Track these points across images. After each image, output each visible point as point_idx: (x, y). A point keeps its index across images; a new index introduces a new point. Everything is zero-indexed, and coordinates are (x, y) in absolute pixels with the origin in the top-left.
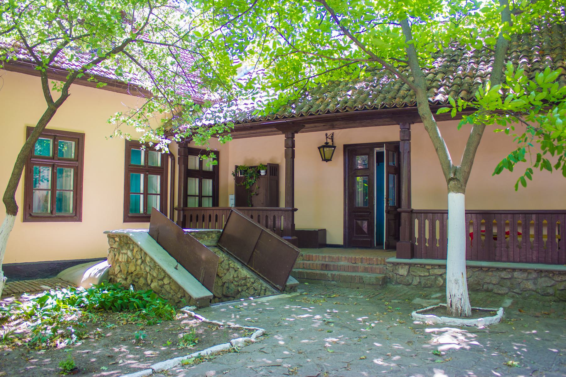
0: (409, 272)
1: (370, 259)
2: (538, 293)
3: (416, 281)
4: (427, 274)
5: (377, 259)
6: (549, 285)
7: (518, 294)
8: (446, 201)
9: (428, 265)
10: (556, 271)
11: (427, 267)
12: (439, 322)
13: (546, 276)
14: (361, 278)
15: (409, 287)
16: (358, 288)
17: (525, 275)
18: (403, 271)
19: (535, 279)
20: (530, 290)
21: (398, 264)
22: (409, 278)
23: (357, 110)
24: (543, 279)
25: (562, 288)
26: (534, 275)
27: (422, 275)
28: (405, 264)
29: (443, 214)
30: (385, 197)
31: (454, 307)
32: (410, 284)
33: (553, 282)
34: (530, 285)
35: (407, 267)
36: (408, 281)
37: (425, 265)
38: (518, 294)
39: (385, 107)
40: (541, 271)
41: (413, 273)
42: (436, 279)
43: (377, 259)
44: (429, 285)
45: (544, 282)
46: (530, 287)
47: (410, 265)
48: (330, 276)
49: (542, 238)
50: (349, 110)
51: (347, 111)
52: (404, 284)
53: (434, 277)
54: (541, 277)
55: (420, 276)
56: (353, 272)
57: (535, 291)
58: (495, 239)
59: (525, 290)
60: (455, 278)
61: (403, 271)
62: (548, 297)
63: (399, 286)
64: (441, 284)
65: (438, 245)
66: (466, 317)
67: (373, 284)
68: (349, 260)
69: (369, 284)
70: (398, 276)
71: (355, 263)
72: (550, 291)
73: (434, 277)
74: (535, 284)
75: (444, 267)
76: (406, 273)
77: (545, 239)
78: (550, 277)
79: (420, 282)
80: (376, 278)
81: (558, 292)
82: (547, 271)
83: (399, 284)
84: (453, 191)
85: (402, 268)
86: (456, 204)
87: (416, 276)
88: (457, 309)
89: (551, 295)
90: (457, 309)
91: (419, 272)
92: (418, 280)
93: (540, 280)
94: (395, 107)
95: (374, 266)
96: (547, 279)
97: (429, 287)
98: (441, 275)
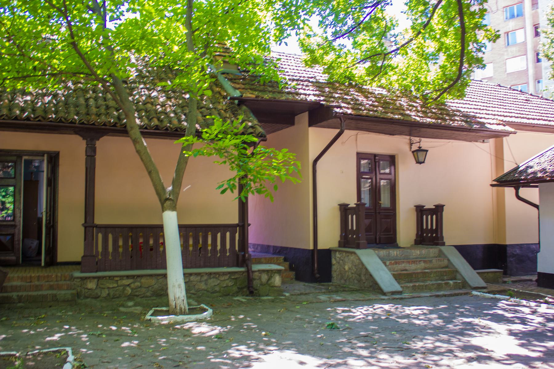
0: (97, 285)
1: (48, 276)
2: (208, 291)
3: (105, 293)
4: (115, 285)
5: (57, 276)
6: (216, 284)
7: (194, 294)
8: (161, 218)
9: (117, 276)
10: (221, 272)
11: (116, 279)
12: (178, 320)
13: (213, 277)
14: (55, 296)
15: (98, 299)
16: (50, 307)
17: (199, 278)
18: (91, 285)
19: (206, 280)
20: (203, 290)
21: (86, 278)
22: (98, 291)
23: (51, 121)
24: (212, 280)
25: (225, 285)
26: (205, 277)
27: (111, 286)
28: (94, 278)
29: (160, 228)
30: (44, 210)
31: (178, 308)
32: (98, 297)
33: (219, 282)
34: (203, 286)
35: (96, 280)
36: (97, 294)
37: (114, 277)
38: (194, 294)
39: (83, 123)
40: (210, 274)
41: (102, 286)
42: (124, 289)
43: (57, 276)
44: (118, 295)
45: (213, 282)
46: (203, 288)
47: (99, 278)
48: (16, 298)
49: (207, 247)
50: (42, 119)
51: (39, 121)
52: (92, 298)
53: (122, 288)
54: (210, 278)
55: (108, 288)
56: (36, 291)
57: (206, 290)
58: (151, 250)
59: (198, 290)
60: (178, 283)
61: (91, 285)
62: (215, 294)
63: (89, 300)
64: (129, 293)
65: (110, 258)
66: (185, 314)
67: (68, 301)
68: (22, 279)
69: (64, 301)
70: (87, 291)
71: (31, 282)
72: (217, 289)
73: (122, 288)
74: (206, 284)
75: (165, 276)
76: (94, 287)
77: (210, 248)
78: (216, 278)
79: (109, 294)
80: (72, 294)
81: (222, 289)
82: (215, 273)
83: (87, 298)
84: (169, 209)
85: (90, 282)
86: (170, 221)
87: (104, 288)
88: (181, 309)
89: (217, 292)
90: (181, 309)
91: (108, 285)
92: (107, 292)
93: (210, 281)
94: (93, 124)
95: (60, 283)
96: (215, 279)
97: (118, 297)
98: (128, 285)
